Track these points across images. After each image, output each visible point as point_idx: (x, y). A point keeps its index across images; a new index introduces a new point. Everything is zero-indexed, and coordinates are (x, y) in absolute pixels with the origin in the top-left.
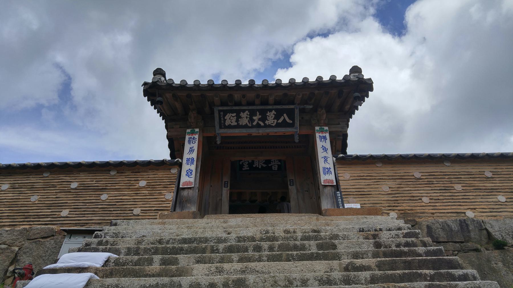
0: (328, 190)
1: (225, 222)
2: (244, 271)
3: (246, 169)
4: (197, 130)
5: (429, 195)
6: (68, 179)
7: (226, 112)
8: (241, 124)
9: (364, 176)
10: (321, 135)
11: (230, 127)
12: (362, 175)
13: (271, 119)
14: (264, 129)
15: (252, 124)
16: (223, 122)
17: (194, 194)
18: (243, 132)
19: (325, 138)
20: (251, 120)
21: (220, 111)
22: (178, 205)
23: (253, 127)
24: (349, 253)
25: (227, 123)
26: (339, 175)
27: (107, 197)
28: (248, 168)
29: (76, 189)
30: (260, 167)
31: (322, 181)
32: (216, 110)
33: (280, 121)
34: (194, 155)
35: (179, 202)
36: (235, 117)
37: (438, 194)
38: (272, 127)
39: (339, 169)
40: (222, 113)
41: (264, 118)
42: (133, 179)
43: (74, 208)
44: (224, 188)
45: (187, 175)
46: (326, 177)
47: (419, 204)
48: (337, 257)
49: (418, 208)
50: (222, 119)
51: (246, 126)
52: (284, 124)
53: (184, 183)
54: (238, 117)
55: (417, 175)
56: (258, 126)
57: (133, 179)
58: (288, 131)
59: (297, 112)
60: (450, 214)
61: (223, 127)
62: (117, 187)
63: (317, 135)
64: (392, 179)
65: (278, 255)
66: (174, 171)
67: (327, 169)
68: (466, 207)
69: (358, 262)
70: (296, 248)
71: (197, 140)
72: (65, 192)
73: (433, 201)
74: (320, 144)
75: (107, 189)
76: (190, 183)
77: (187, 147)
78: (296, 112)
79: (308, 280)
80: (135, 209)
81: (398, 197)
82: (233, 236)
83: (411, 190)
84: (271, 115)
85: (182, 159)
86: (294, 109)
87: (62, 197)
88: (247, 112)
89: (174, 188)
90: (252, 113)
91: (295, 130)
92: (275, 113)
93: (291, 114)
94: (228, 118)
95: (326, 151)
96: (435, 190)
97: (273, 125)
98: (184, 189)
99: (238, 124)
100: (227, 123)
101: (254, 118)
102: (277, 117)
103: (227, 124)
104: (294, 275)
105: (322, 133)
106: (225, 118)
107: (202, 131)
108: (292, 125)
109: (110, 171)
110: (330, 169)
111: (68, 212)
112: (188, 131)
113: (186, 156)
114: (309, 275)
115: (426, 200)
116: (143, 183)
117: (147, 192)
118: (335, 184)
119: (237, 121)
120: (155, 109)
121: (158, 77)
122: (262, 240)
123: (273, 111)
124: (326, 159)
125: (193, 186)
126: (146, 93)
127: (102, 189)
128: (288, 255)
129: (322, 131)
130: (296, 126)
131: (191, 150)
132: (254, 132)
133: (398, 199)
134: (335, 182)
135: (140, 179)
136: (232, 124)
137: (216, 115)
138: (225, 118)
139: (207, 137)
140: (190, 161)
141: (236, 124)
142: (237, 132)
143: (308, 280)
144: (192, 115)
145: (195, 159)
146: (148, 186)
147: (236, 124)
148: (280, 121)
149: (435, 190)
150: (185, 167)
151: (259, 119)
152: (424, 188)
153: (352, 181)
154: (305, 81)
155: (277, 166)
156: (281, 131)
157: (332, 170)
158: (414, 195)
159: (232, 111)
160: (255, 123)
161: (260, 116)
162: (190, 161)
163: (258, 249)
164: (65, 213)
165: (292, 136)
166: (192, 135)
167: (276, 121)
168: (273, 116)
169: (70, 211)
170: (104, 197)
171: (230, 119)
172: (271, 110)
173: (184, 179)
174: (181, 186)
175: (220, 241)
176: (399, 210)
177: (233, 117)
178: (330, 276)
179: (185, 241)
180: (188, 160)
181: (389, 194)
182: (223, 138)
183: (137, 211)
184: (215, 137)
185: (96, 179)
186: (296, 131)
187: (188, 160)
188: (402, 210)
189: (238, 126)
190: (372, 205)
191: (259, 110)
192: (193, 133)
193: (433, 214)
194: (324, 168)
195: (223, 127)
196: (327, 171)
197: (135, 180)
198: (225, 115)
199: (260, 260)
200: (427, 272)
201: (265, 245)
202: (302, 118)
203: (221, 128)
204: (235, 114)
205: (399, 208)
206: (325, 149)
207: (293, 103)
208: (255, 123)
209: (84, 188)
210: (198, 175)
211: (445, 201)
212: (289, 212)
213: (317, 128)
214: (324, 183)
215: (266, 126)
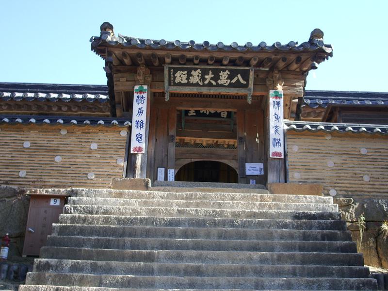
3: (192, 114)
4: (145, 87)
6: (19, 137)
7: (176, 70)
8: (191, 82)
11: (180, 84)
13: (224, 78)
14: (216, 88)
15: (203, 83)
16: (172, 79)
18: (194, 90)
19: (278, 104)
20: (203, 79)
21: (170, 69)
23: (204, 85)
25: (177, 81)
26: (289, 147)
28: (195, 114)
31: (271, 154)
33: (233, 81)
34: (143, 117)
36: (186, 75)
38: (225, 86)
40: (172, 71)
41: (216, 78)
42: (84, 140)
43: (31, 169)
50: (172, 76)
51: (197, 85)
52: (238, 85)
54: (189, 75)
55: (364, 151)
56: (210, 85)
57: (84, 140)
58: (242, 92)
59: (252, 74)
61: (172, 84)
62: (69, 148)
67: (277, 140)
71: (146, 99)
72: (18, 151)
74: (272, 110)
75: (59, 150)
77: (136, 107)
85: (131, 122)
86: (249, 70)
87: (17, 157)
88: (199, 71)
90: (204, 72)
92: (229, 73)
93: (246, 76)
95: (278, 119)
97: (226, 85)
99: (189, 82)
100: (177, 81)
101: (206, 77)
102: (230, 77)
106: (176, 75)
107: (151, 87)
108: (246, 86)
110: (280, 140)
111: (25, 173)
112: (137, 87)
113: (135, 118)
116: (94, 146)
118: (283, 157)
119: (188, 79)
120: (94, 52)
123: (227, 71)
126: (94, 48)
130: (250, 86)
131: (140, 112)
132: (205, 91)
134: (283, 155)
136: (182, 82)
138: (176, 75)
140: (140, 124)
141: (186, 81)
144: (142, 70)
145: (145, 122)
147: (186, 81)
148: (233, 81)
150: (135, 131)
151: (212, 79)
153: (302, 154)
154: (263, 46)
155: (226, 113)
156: (233, 91)
157: (282, 142)
159: (183, 69)
160: (206, 82)
161: (213, 76)
162: (140, 124)
167: (229, 81)
168: (227, 76)
169: (27, 172)
170: (58, 159)
171: (181, 77)
172: (224, 70)
177: (184, 75)
178: (262, 267)
180: (137, 122)
182: (172, 95)
185: (48, 138)
186: (250, 92)
187: (137, 122)
189: (189, 84)
190: (315, 181)
191: (212, 70)
192: (141, 91)
194: (274, 139)
195: (172, 84)
196: (277, 142)
198: (175, 73)
202: (257, 76)
203: (170, 84)
204: (186, 72)
208: (206, 82)
209: (37, 148)
212: (236, 182)
214: (272, 155)
215: (218, 85)
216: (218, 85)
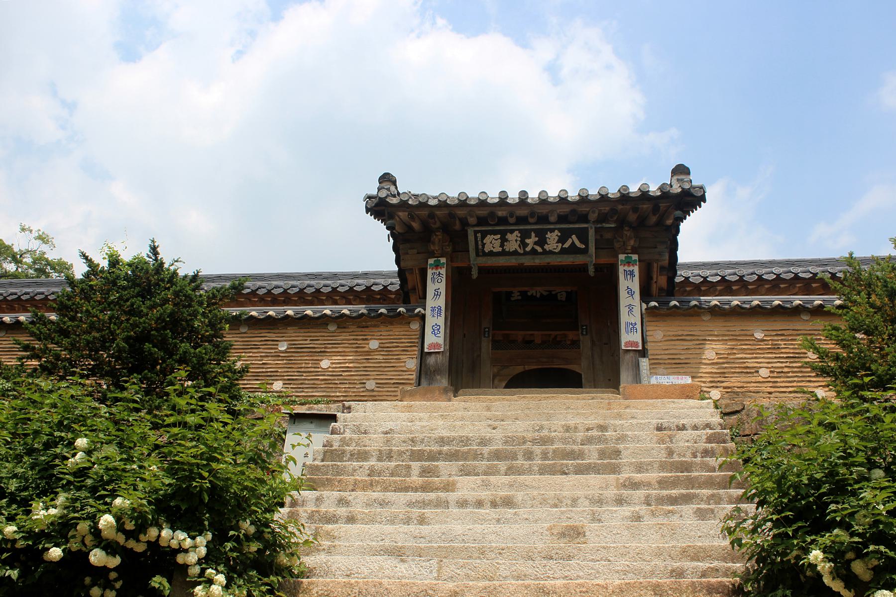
0: (628, 357)
1: (489, 409)
2: (512, 486)
4: (443, 260)
5: (770, 365)
6: (272, 336)
7: (484, 234)
9: (682, 335)
10: (626, 268)
11: (491, 254)
12: (680, 333)
16: (480, 247)
17: (442, 361)
18: (512, 261)
19: (632, 273)
21: (476, 232)
22: (423, 376)
24: (631, 464)
26: (648, 333)
27: (329, 365)
28: (520, 298)
29: (285, 352)
30: (538, 296)
31: (623, 344)
32: (471, 232)
33: (566, 245)
35: (425, 373)
37: (784, 365)
39: (648, 324)
40: (479, 235)
41: (542, 242)
44: (483, 338)
45: (433, 332)
46: (629, 337)
47: (753, 379)
48: (614, 469)
49: (753, 384)
50: (480, 243)
51: (515, 253)
53: (431, 346)
54: (504, 240)
58: (579, 259)
60: (792, 395)
62: (340, 350)
63: (621, 269)
64: (722, 340)
65: (551, 465)
66: (415, 326)
68: (816, 384)
69: (638, 477)
70: (571, 455)
71: (444, 276)
73: (775, 375)
76: (437, 345)
78: (590, 234)
79: (579, 498)
80: (368, 382)
81: (726, 368)
82: (498, 434)
83: (745, 358)
84: (553, 238)
86: (587, 228)
88: (516, 233)
89: (416, 351)
90: (525, 235)
91: (588, 259)
93: (584, 238)
94: (489, 241)
96: (780, 357)
98: (430, 354)
99: (503, 250)
101: (527, 241)
102: (562, 240)
103: (487, 250)
104: (565, 493)
105: (629, 265)
107: (451, 259)
108: (585, 251)
109: (327, 325)
112: (431, 261)
114: (579, 493)
115: (764, 372)
116: (374, 344)
117: (381, 357)
118: (640, 348)
119: (502, 245)
121: (386, 185)
122: (534, 441)
124: (630, 308)
125: (442, 350)
127: (321, 352)
128: (562, 464)
129: (629, 263)
131: (437, 294)
132: (527, 261)
133: (725, 371)
134: (640, 345)
135: (369, 337)
136: (495, 250)
137: (471, 238)
139: (458, 267)
142: (502, 261)
143: (579, 498)
144: (438, 237)
145: (443, 308)
146: (382, 347)
148: (566, 245)
149: (780, 357)
150: (430, 321)
152: (766, 355)
155: (564, 294)
156: (568, 260)
158: (747, 365)
159: (494, 233)
160: (528, 249)
161: (537, 239)
162: (436, 310)
163: (529, 455)
164: (278, 386)
165: (583, 268)
166: (437, 269)
167: (560, 245)
168: (557, 238)
171: (492, 243)
172: (552, 231)
173: (430, 339)
174: (426, 350)
175: (483, 442)
176: (725, 388)
179: (442, 441)
181: (717, 363)
183: (371, 385)
184: (469, 269)
186: (591, 259)
188: (729, 388)
189: (504, 253)
191: (535, 231)
192: (437, 266)
193: (770, 393)
194: (627, 324)
197: (363, 340)
198: (483, 238)
199: (530, 471)
200: (705, 491)
201: (537, 449)
203: (477, 255)
204: (499, 236)
205: (725, 384)
206: (631, 293)
207: (586, 221)
208: (528, 249)
210: (448, 331)
211: (790, 374)
213: (622, 257)
216: (545, 252)
